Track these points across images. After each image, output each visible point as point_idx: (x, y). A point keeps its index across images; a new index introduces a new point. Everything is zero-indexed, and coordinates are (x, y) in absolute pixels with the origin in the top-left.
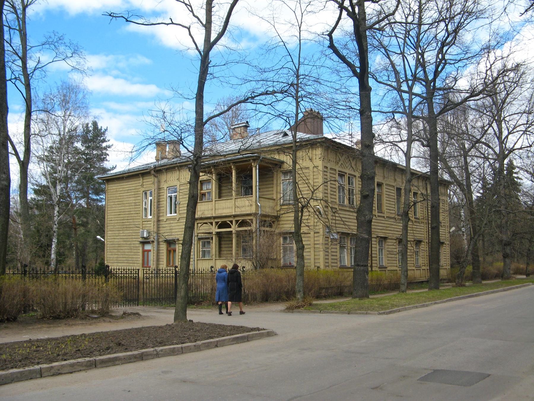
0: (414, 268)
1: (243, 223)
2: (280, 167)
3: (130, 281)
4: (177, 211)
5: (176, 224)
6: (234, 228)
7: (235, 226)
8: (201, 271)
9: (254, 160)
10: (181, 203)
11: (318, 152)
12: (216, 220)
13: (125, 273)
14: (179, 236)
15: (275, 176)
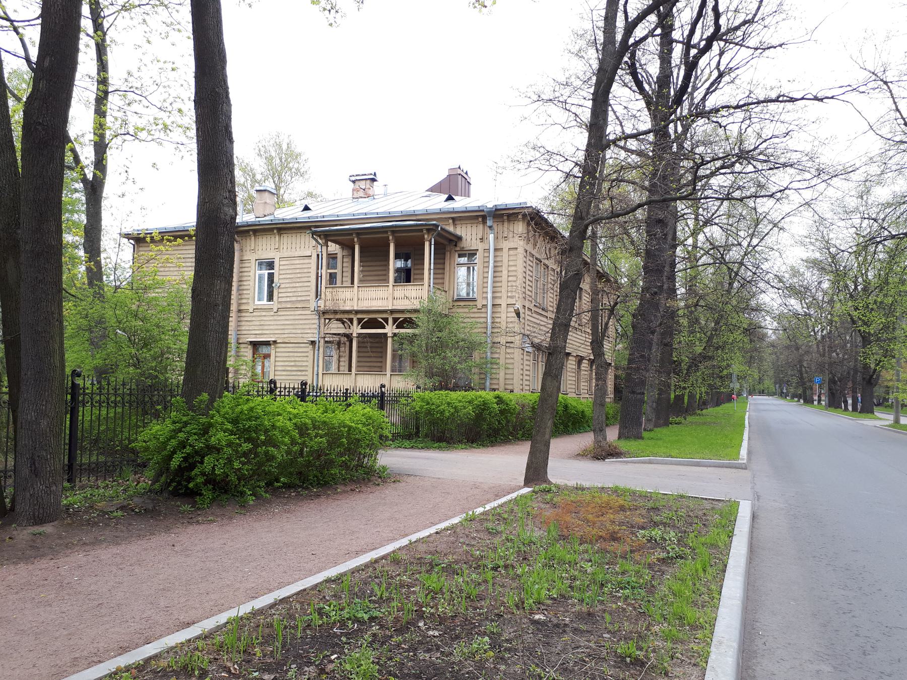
1: (373, 323)
2: (456, 245)
4: (275, 298)
5: (271, 318)
6: (390, 329)
9: (429, 230)
10: (283, 286)
11: (520, 227)
12: (360, 316)
13: (287, 394)
14: (277, 336)
15: (448, 254)
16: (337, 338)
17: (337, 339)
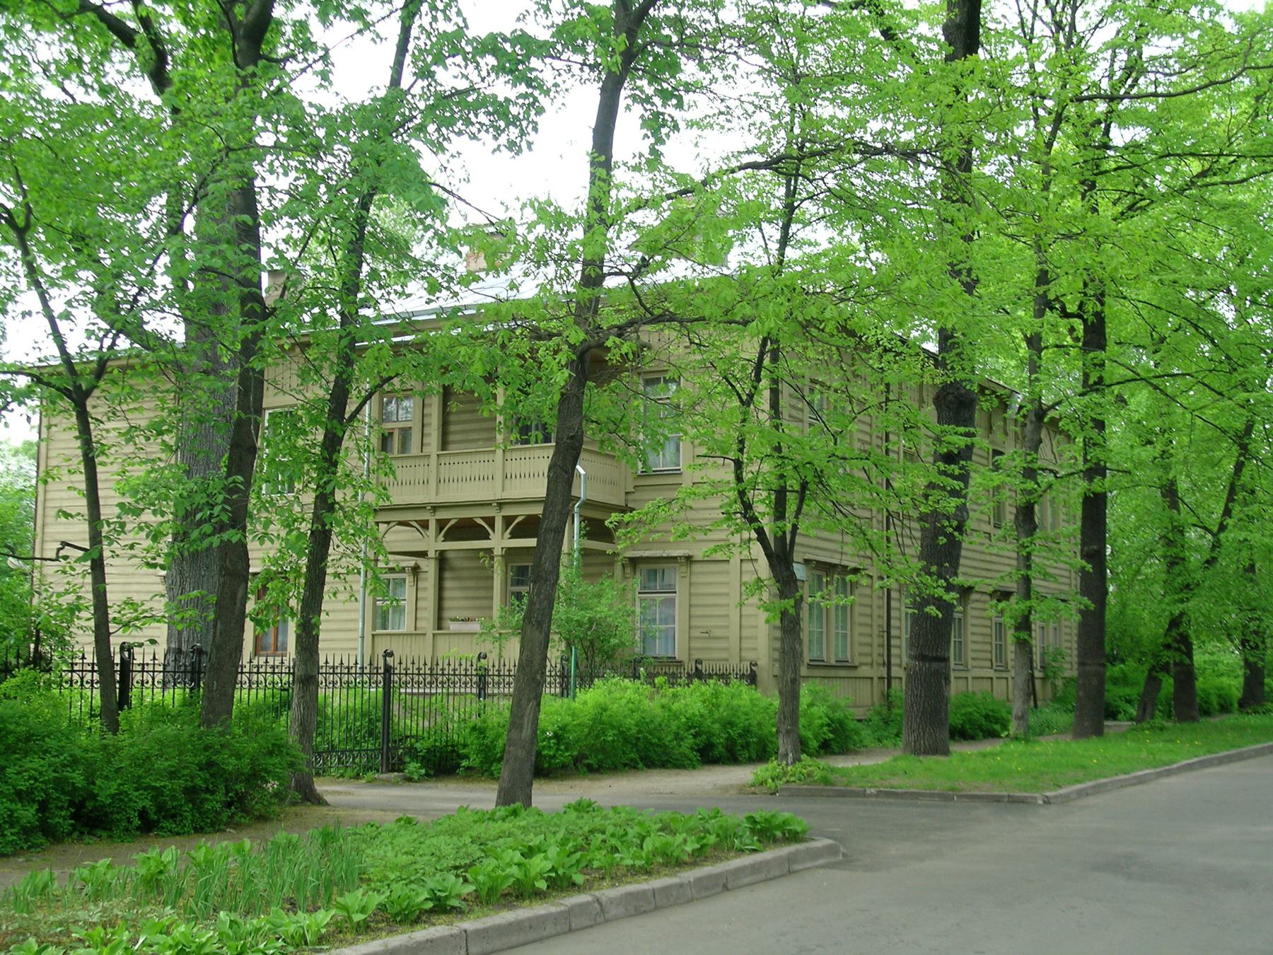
0: (991, 673)
3: (373, 696)
6: (499, 541)
7: (437, 536)
8: (440, 667)
16: (410, 562)
17: (412, 564)
